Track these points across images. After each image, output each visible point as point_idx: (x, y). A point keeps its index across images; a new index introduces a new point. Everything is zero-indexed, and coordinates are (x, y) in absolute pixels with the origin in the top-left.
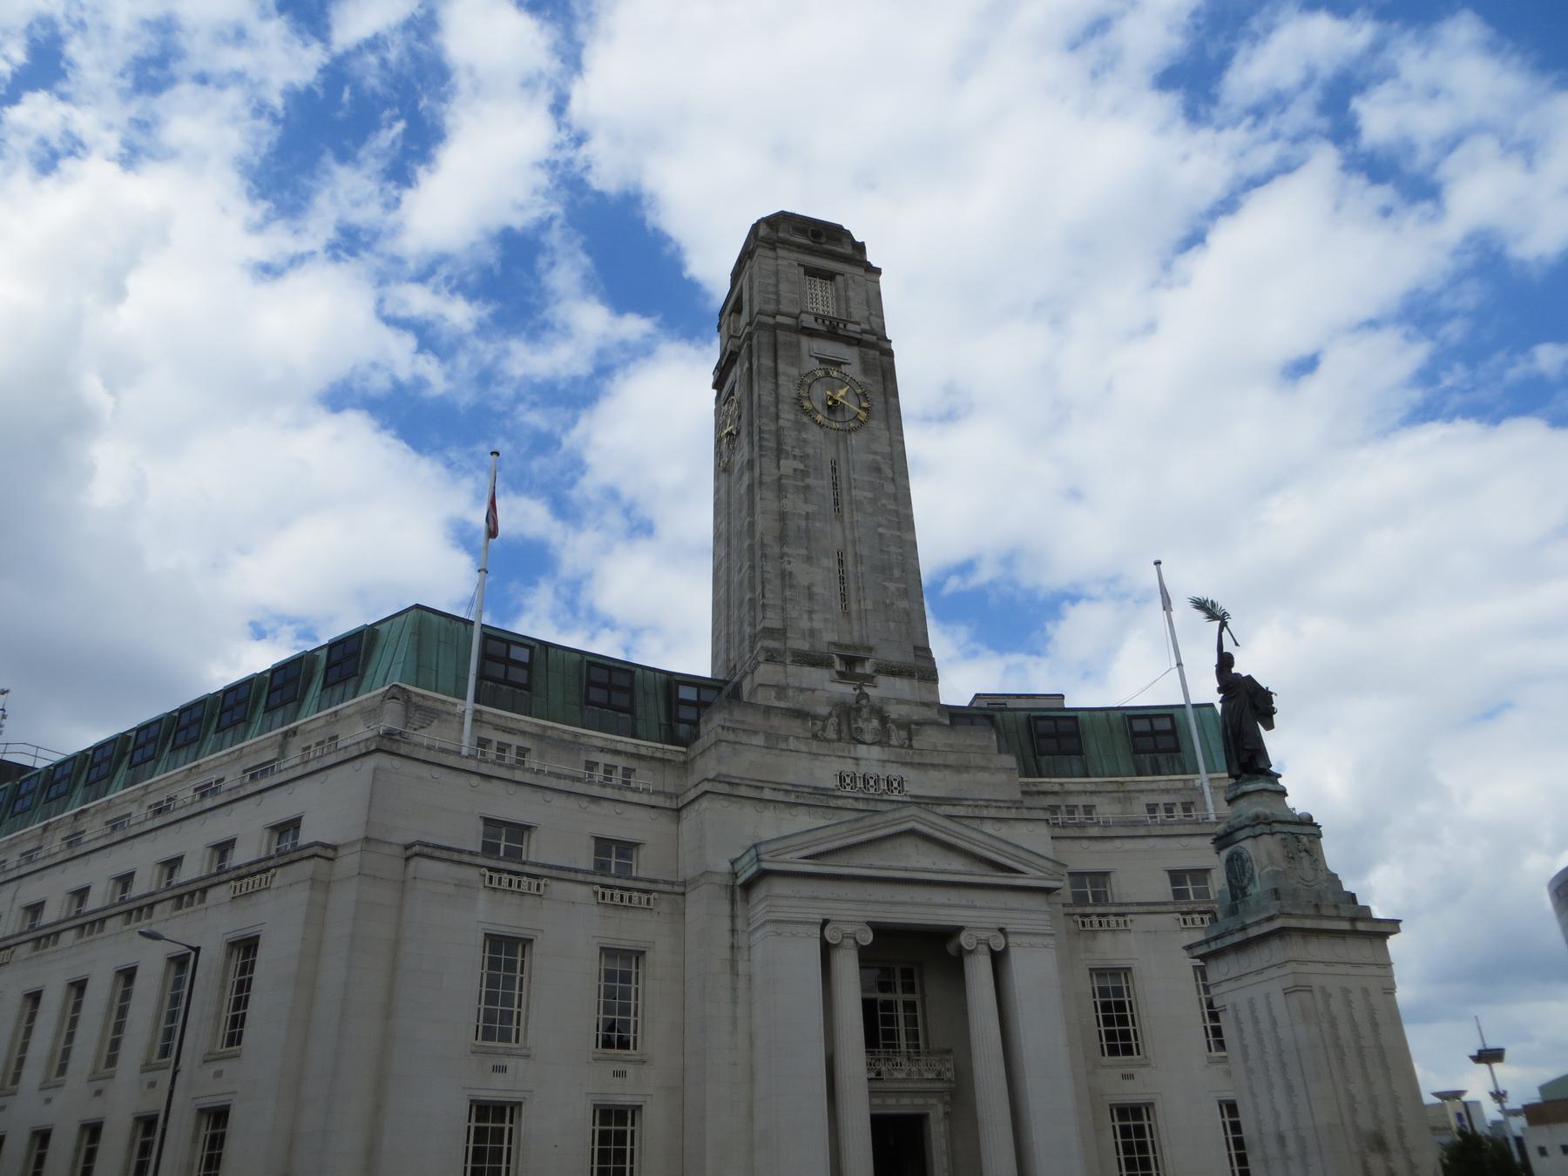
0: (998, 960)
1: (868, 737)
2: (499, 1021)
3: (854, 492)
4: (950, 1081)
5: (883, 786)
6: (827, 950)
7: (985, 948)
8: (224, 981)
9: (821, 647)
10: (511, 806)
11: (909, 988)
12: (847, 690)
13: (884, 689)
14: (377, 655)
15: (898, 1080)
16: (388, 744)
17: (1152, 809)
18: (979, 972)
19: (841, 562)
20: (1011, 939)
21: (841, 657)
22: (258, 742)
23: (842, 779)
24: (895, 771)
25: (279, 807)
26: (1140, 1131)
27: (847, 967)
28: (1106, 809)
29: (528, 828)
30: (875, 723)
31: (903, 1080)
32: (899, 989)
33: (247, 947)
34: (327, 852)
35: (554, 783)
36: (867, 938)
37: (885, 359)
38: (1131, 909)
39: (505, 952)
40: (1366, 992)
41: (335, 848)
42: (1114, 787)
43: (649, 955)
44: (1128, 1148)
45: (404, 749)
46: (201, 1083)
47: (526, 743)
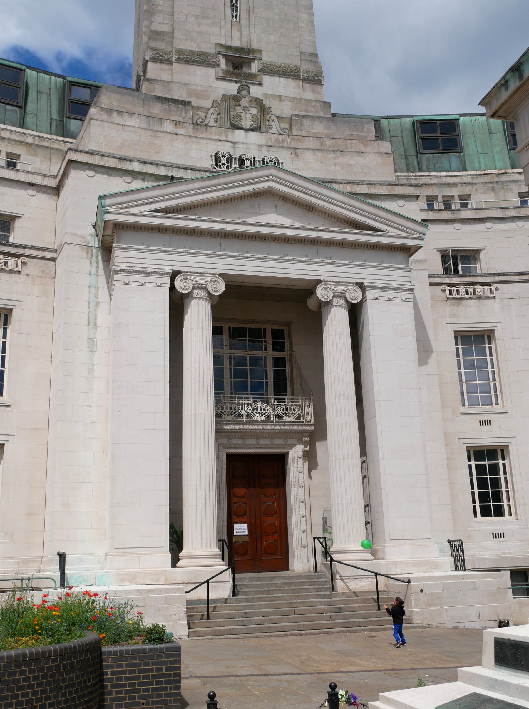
0: (355, 312)
4: (309, 424)
6: (178, 305)
7: (342, 302)
9: (209, 48)
12: (232, 88)
13: (270, 88)
15: (285, 423)
18: (336, 327)
20: (368, 293)
23: (217, 159)
26: (494, 469)
27: (199, 320)
28: (480, 198)
30: (254, 111)
31: (262, 423)
32: (269, 347)
36: (220, 288)
38: (497, 279)
43: (15, 315)
44: (482, 484)
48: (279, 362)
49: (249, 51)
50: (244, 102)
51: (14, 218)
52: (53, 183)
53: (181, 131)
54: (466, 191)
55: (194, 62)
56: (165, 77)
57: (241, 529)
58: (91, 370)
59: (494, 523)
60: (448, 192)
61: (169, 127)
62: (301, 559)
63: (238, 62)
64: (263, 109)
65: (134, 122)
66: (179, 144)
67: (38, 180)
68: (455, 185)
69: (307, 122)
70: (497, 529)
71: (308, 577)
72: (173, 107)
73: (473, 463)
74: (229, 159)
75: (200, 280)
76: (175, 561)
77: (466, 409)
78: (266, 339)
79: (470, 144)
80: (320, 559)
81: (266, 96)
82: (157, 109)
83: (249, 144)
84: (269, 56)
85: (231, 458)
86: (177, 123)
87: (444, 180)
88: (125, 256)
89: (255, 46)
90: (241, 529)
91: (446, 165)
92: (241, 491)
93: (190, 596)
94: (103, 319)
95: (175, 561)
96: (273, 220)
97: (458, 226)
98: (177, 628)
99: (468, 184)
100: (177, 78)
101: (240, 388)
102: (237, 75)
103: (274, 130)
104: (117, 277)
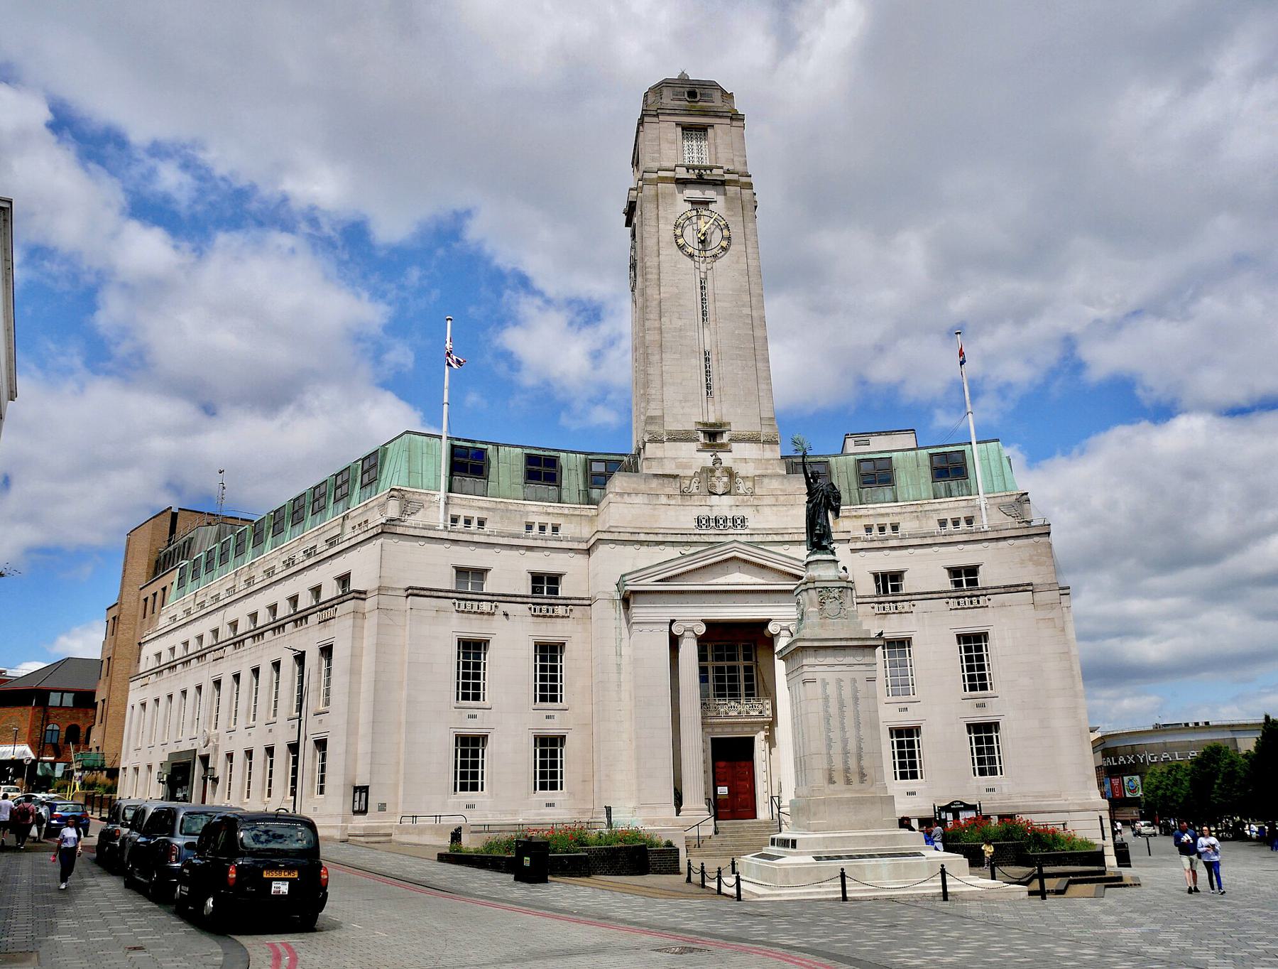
1: (720, 490)
2: (470, 686)
3: (718, 304)
5: (730, 524)
6: (674, 642)
8: (320, 669)
9: (691, 427)
10: (472, 558)
11: (747, 658)
12: (706, 459)
14: (387, 463)
16: (387, 530)
17: (943, 523)
19: (707, 360)
21: (705, 432)
22: (330, 522)
23: (699, 521)
24: (738, 513)
25: (339, 566)
26: (911, 744)
27: (689, 650)
28: (907, 526)
29: (487, 570)
30: (725, 479)
32: (741, 657)
33: (327, 651)
34: (361, 595)
35: (501, 541)
36: (702, 629)
37: (746, 192)
39: (472, 649)
40: (854, 680)
41: (365, 592)
42: (913, 509)
45: (399, 530)
46: (314, 728)
47: (483, 515)
48: (748, 669)
49: (721, 425)
50: (718, 473)
51: (561, 575)
52: (584, 546)
53: (672, 502)
54: (895, 520)
55: (681, 440)
56: (659, 454)
57: (723, 790)
58: (619, 686)
59: (909, 784)
60: (882, 521)
61: (664, 500)
62: (763, 813)
63: (713, 435)
64: (731, 474)
65: (639, 499)
66: (672, 512)
67: (575, 545)
68: (888, 514)
69: (766, 481)
70: (910, 789)
71: (766, 822)
72: (666, 480)
73: (895, 740)
74: (708, 520)
75: (689, 625)
76: (678, 812)
77: (891, 699)
78: (735, 655)
79: (902, 478)
80: (776, 811)
81: (735, 460)
82: (655, 483)
83: (723, 506)
84: (737, 427)
85: (717, 743)
86: (669, 496)
87: (879, 511)
88: (640, 611)
89: (725, 420)
90: (723, 790)
91: (881, 497)
92: (722, 764)
93: (687, 834)
94: (625, 651)
95: (678, 812)
96: (738, 579)
97: (887, 552)
98: (680, 845)
99: (898, 514)
100: (669, 454)
101: (720, 692)
102: (713, 446)
103: (741, 491)
104: (635, 627)
